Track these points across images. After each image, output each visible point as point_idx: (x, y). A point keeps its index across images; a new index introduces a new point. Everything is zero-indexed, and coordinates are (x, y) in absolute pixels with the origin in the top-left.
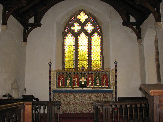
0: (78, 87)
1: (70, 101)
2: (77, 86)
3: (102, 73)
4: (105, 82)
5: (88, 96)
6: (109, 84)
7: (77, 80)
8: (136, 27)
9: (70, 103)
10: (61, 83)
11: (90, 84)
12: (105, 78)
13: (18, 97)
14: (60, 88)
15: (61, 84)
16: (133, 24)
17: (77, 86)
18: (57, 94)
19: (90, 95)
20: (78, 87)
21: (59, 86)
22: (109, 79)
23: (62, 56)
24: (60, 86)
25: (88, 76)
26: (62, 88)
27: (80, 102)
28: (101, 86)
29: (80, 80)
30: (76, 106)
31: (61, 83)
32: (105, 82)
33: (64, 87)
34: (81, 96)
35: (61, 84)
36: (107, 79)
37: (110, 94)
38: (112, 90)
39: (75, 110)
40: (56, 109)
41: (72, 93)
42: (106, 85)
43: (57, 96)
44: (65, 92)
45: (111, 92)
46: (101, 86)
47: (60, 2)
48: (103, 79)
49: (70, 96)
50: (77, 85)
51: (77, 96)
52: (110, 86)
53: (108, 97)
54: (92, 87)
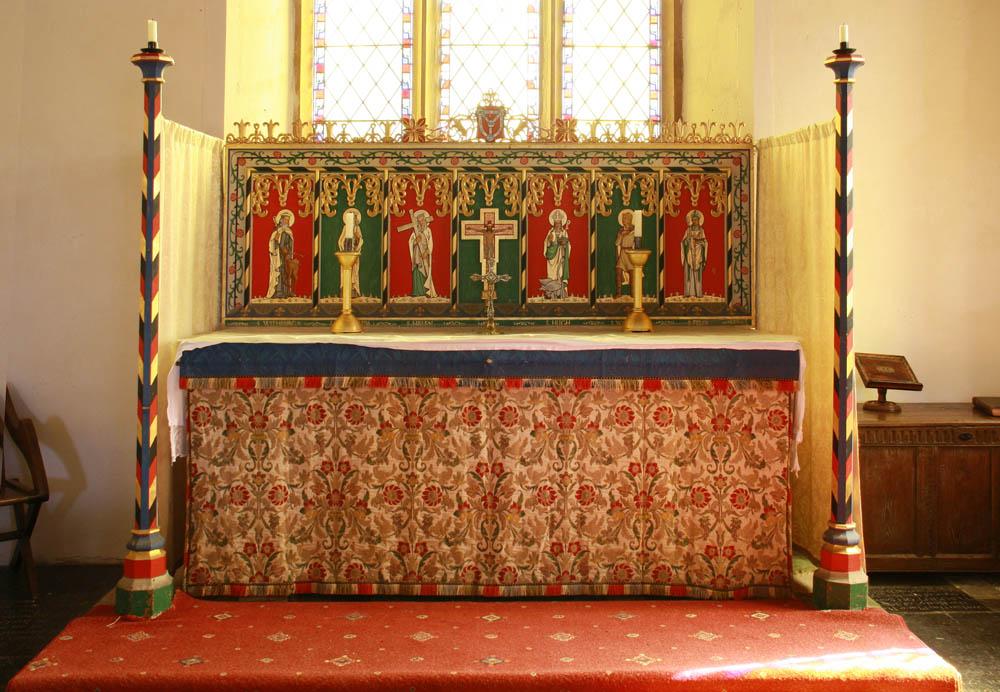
0: (445, 300)
1: (355, 460)
3: (675, 163)
4: (694, 256)
6: (730, 276)
7: (428, 232)
9: (354, 490)
10: (276, 262)
11: (555, 270)
12: (421, 217)
14: (271, 311)
15: (274, 278)
17: (435, 298)
19: (568, 401)
20: (445, 300)
21: (264, 295)
22: (735, 225)
24: (271, 291)
25: (534, 198)
26: (289, 311)
27: (612, 478)
28: (385, 301)
29: (456, 228)
30: (728, 520)
32: (694, 256)
33: (715, 306)
34: (625, 417)
36: (715, 230)
37: (774, 397)
39: (722, 564)
41: (384, 384)
42: (707, 290)
43: (221, 415)
44: (318, 364)
45: (781, 368)
46: (385, 301)
49: (355, 415)
50: (429, 284)
51: (432, 412)
53: (748, 428)
54: (572, 299)
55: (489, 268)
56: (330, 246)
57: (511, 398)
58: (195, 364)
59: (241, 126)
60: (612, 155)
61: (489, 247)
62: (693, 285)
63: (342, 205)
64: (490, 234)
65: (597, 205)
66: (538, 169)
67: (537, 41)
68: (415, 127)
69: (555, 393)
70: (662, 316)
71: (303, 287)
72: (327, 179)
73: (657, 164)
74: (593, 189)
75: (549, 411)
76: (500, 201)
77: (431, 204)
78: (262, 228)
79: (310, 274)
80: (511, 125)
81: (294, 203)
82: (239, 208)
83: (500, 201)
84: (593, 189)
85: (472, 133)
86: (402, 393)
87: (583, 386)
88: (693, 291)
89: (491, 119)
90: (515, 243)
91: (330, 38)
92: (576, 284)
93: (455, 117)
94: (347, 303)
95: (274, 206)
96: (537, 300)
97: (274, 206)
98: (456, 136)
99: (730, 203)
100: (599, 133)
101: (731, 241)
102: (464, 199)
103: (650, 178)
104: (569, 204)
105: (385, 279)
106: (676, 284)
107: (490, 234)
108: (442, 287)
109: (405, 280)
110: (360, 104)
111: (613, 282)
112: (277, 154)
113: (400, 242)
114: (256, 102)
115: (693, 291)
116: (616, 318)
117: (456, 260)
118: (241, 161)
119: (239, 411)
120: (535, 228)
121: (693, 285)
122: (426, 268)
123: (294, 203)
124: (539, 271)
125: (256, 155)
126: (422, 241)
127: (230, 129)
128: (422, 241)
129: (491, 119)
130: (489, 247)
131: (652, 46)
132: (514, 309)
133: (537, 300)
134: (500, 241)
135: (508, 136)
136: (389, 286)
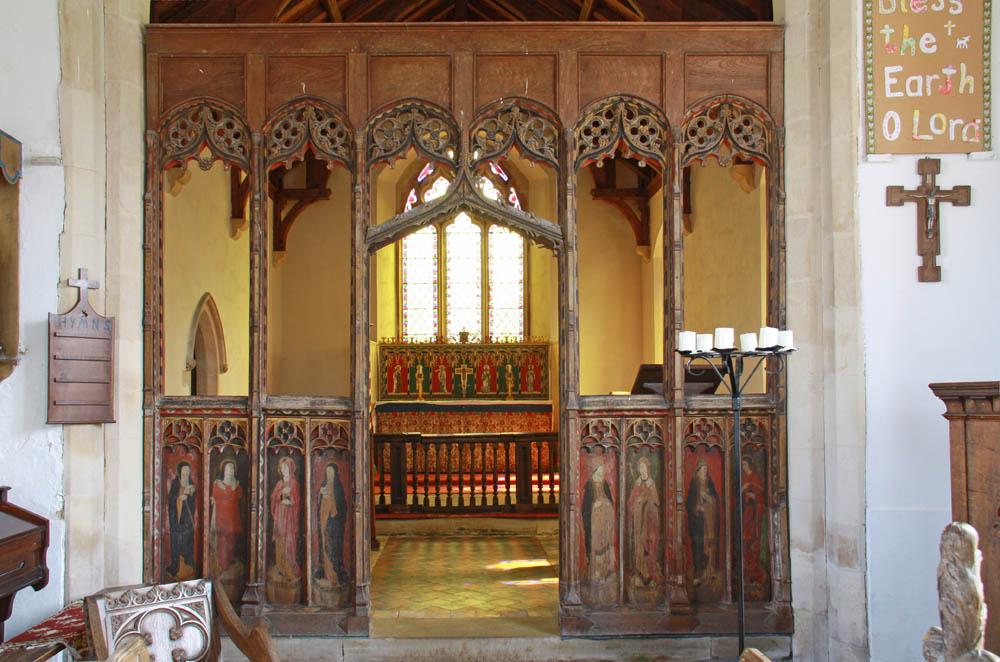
2: (446, 393)
4: (531, 379)
5: (393, 421)
6: (542, 385)
7: (444, 372)
8: (891, 35)
10: (395, 382)
11: (485, 384)
13: (69, 431)
15: (395, 387)
16: (629, 192)
17: (446, 393)
18: (387, 417)
23: (445, 244)
31: (395, 382)
32: (531, 379)
35: (395, 387)
36: (538, 370)
37: (545, 417)
38: (551, 405)
40: (385, 460)
42: (535, 389)
47: (241, 650)
48: (524, 370)
52: (547, 390)
55: (464, 382)
56: (413, 376)
57: (470, 418)
58: (379, 409)
59: (384, 339)
60: (506, 348)
61: (464, 376)
62: (530, 388)
63: (416, 364)
64: (464, 373)
65: (498, 363)
66: (480, 352)
67: (558, 536)
68: (441, 337)
69: (482, 416)
70: (516, 397)
71: (405, 390)
72: (412, 356)
73: (518, 350)
74: (497, 358)
75: (481, 421)
76: (467, 362)
77: (445, 363)
78: (391, 371)
79: (407, 386)
80: (470, 338)
81: (401, 363)
82: (384, 364)
83: (467, 362)
84: (497, 358)
85: (458, 338)
86: (439, 417)
87: (489, 415)
88: (530, 391)
89: (464, 336)
90: (472, 376)
91: (408, 306)
92: (492, 388)
93: (453, 336)
94: (420, 393)
95: (394, 364)
96: (480, 393)
97: (394, 364)
98: (453, 342)
99: (542, 362)
100: (499, 341)
101: (542, 374)
102: (456, 361)
103: (404, 355)
104: (490, 363)
105: (431, 387)
106: (525, 388)
107: (464, 373)
108: (449, 390)
109: (438, 387)
110: (420, 329)
111: (503, 381)
112: (395, 347)
113: (435, 375)
114: (386, 331)
115: (530, 391)
116: (504, 397)
117: (454, 381)
118: (383, 350)
119: (393, 421)
120: (479, 370)
121: (530, 388)
122: (444, 384)
123: (401, 363)
124: (480, 384)
125: (388, 348)
126: (443, 374)
127: (379, 339)
128: (443, 374)
129: (464, 336)
130: (464, 376)
131: (520, 308)
132: (471, 395)
133: (480, 393)
134: (892, 91)
135: (470, 341)
136: (432, 386)
